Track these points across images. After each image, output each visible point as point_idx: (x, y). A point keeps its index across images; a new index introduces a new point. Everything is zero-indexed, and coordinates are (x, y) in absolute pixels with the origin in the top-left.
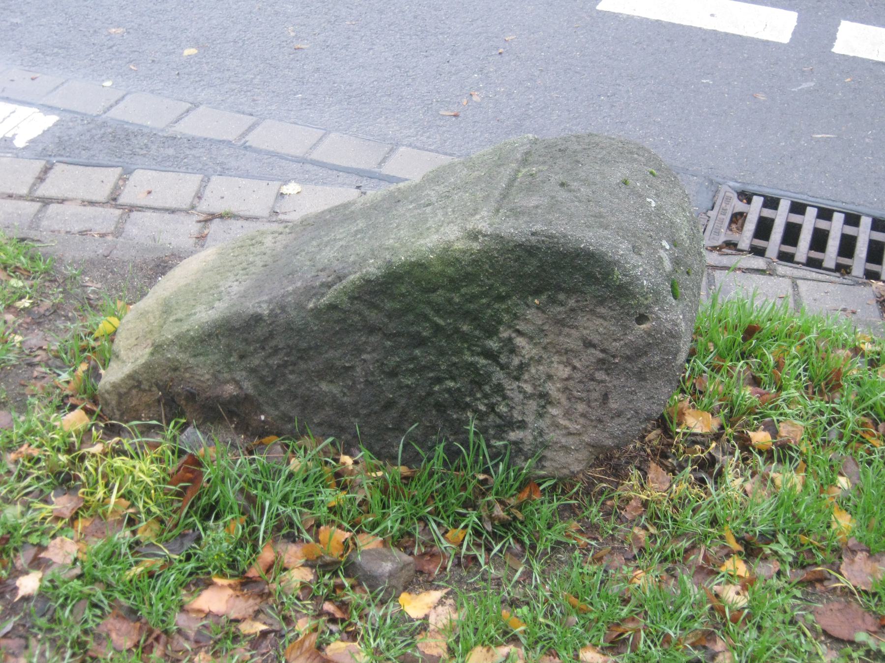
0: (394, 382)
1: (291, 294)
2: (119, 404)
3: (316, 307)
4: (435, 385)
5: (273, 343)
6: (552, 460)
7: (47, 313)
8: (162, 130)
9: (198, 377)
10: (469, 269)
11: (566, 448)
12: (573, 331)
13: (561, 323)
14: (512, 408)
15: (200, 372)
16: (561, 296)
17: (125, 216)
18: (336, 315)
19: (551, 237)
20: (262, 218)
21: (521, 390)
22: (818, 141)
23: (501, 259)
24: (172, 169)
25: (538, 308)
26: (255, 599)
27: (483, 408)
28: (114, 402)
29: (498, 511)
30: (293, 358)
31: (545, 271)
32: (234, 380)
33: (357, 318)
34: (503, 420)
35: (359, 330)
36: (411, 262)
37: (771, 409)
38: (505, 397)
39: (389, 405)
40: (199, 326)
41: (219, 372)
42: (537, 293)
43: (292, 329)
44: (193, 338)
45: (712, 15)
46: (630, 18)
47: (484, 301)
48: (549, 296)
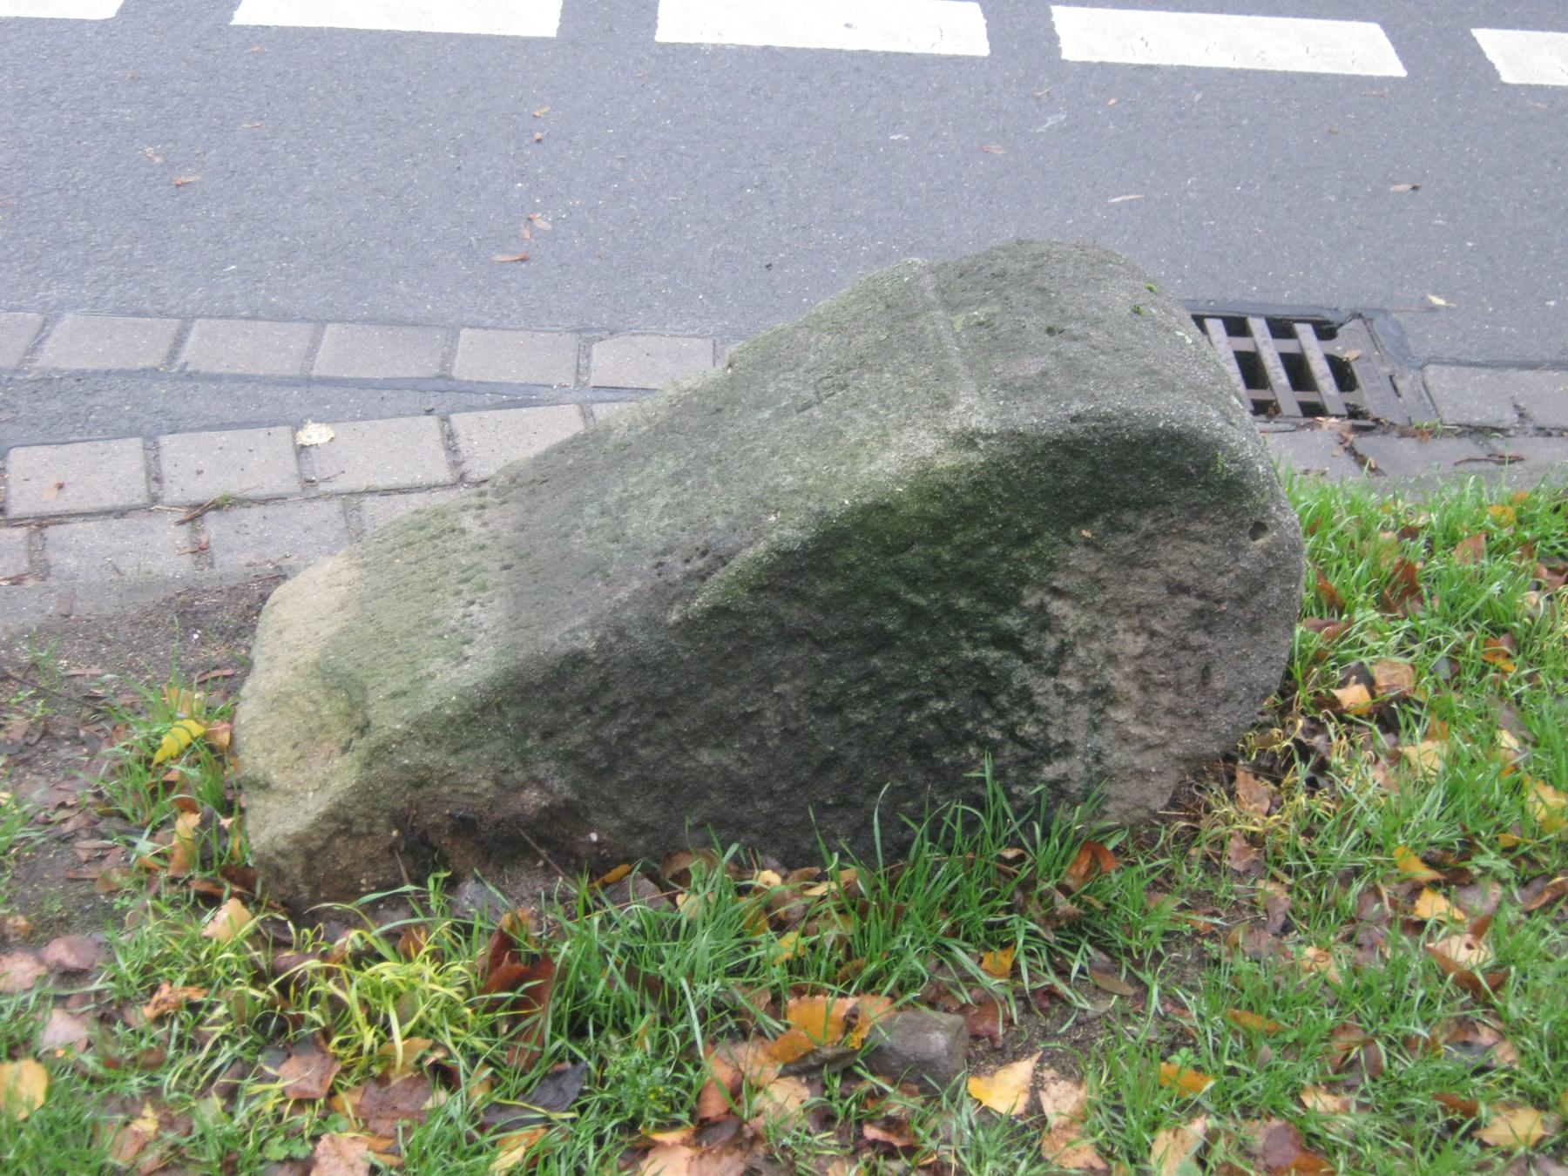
0: (835, 722)
1: (627, 604)
2: (309, 869)
3: (686, 618)
4: (910, 713)
5: (608, 699)
6: (1117, 798)
7: (34, 740)
8: (17, 371)
9: (466, 789)
10: (968, 499)
11: (1142, 775)
12: (1150, 573)
13: (1131, 562)
14: (1047, 724)
15: (470, 778)
16: (1128, 517)
17: (36, 537)
18: (726, 626)
19: (1106, 418)
20: (292, 495)
21: (1061, 691)
22: (1119, 207)
23: (1023, 472)
24: (76, 437)
25: (1088, 543)
26: (730, 1154)
27: (996, 735)
28: (297, 871)
29: (1063, 905)
30: (647, 718)
31: (1100, 478)
32: (533, 779)
33: (764, 623)
34: (1032, 749)
35: (769, 644)
36: (865, 506)
37: (1345, 647)
38: (1032, 708)
39: (830, 762)
40: (460, 696)
41: (506, 771)
42: (1086, 518)
43: (643, 666)
44: (451, 720)
45: (848, 26)
46: (718, 50)
47: (994, 549)
48: (1109, 520)
